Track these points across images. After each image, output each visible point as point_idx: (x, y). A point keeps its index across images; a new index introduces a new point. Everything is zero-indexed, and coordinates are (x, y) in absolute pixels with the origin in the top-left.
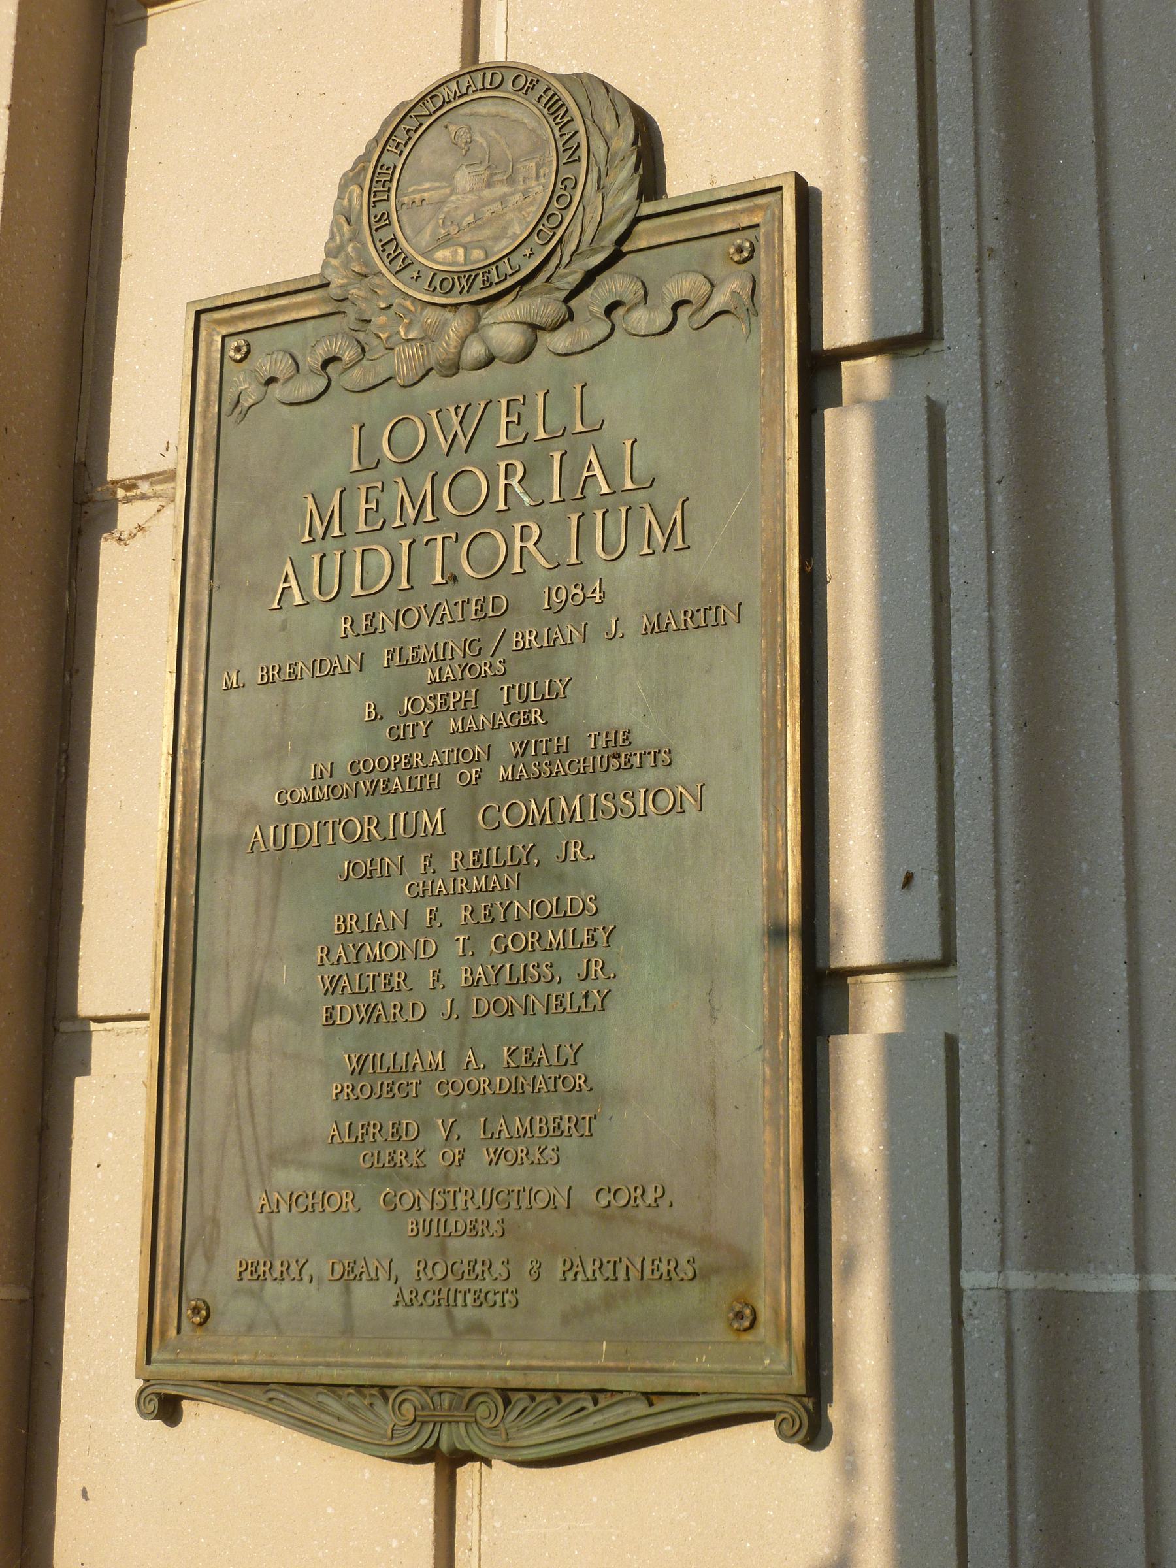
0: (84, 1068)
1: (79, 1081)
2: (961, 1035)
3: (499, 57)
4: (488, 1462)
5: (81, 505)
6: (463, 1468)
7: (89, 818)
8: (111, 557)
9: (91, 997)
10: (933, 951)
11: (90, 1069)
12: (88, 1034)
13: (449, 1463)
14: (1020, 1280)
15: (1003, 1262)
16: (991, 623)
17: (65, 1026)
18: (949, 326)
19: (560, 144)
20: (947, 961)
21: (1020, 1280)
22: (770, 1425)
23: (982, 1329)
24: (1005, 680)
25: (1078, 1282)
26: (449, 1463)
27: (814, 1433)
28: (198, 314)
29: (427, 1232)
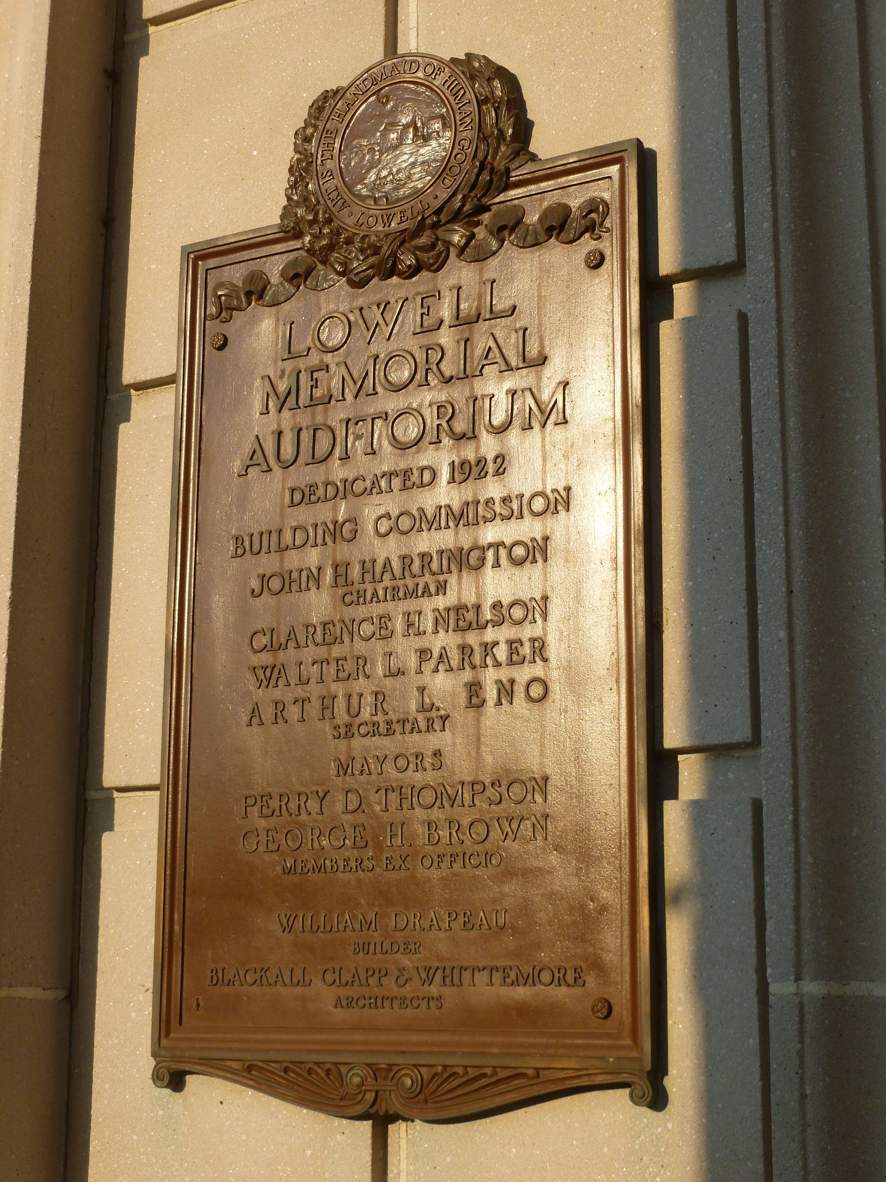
0: (146, 52)
1: (142, 61)
2: (749, 314)
3: (413, 48)
4: (413, 1121)
5: (84, 811)
6: (394, 1125)
7: (107, 736)
8: (111, 846)
9: (115, 771)
10: (744, 733)
11: (148, 50)
12: (111, 801)
13: (382, 1123)
14: (812, 988)
15: (798, 978)
16: (768, 33)
17: (92, 795)
18: (766, 733)
19: (458, 119)
20: (756, 741)
21: (812, 988)
22: (626, 1092)
23: (782, 1026)
24: (786, 260)
25: (857, 988)
26: (382, 1123)
27: (658, 1100)
28: (196, 260)
29: (366, 951)
